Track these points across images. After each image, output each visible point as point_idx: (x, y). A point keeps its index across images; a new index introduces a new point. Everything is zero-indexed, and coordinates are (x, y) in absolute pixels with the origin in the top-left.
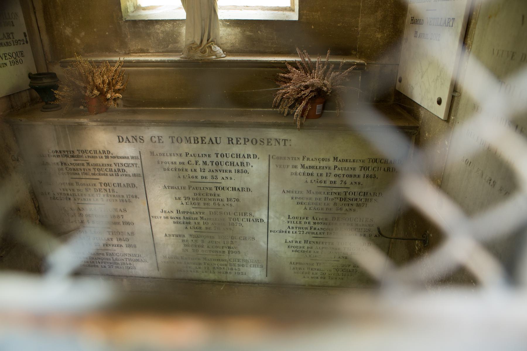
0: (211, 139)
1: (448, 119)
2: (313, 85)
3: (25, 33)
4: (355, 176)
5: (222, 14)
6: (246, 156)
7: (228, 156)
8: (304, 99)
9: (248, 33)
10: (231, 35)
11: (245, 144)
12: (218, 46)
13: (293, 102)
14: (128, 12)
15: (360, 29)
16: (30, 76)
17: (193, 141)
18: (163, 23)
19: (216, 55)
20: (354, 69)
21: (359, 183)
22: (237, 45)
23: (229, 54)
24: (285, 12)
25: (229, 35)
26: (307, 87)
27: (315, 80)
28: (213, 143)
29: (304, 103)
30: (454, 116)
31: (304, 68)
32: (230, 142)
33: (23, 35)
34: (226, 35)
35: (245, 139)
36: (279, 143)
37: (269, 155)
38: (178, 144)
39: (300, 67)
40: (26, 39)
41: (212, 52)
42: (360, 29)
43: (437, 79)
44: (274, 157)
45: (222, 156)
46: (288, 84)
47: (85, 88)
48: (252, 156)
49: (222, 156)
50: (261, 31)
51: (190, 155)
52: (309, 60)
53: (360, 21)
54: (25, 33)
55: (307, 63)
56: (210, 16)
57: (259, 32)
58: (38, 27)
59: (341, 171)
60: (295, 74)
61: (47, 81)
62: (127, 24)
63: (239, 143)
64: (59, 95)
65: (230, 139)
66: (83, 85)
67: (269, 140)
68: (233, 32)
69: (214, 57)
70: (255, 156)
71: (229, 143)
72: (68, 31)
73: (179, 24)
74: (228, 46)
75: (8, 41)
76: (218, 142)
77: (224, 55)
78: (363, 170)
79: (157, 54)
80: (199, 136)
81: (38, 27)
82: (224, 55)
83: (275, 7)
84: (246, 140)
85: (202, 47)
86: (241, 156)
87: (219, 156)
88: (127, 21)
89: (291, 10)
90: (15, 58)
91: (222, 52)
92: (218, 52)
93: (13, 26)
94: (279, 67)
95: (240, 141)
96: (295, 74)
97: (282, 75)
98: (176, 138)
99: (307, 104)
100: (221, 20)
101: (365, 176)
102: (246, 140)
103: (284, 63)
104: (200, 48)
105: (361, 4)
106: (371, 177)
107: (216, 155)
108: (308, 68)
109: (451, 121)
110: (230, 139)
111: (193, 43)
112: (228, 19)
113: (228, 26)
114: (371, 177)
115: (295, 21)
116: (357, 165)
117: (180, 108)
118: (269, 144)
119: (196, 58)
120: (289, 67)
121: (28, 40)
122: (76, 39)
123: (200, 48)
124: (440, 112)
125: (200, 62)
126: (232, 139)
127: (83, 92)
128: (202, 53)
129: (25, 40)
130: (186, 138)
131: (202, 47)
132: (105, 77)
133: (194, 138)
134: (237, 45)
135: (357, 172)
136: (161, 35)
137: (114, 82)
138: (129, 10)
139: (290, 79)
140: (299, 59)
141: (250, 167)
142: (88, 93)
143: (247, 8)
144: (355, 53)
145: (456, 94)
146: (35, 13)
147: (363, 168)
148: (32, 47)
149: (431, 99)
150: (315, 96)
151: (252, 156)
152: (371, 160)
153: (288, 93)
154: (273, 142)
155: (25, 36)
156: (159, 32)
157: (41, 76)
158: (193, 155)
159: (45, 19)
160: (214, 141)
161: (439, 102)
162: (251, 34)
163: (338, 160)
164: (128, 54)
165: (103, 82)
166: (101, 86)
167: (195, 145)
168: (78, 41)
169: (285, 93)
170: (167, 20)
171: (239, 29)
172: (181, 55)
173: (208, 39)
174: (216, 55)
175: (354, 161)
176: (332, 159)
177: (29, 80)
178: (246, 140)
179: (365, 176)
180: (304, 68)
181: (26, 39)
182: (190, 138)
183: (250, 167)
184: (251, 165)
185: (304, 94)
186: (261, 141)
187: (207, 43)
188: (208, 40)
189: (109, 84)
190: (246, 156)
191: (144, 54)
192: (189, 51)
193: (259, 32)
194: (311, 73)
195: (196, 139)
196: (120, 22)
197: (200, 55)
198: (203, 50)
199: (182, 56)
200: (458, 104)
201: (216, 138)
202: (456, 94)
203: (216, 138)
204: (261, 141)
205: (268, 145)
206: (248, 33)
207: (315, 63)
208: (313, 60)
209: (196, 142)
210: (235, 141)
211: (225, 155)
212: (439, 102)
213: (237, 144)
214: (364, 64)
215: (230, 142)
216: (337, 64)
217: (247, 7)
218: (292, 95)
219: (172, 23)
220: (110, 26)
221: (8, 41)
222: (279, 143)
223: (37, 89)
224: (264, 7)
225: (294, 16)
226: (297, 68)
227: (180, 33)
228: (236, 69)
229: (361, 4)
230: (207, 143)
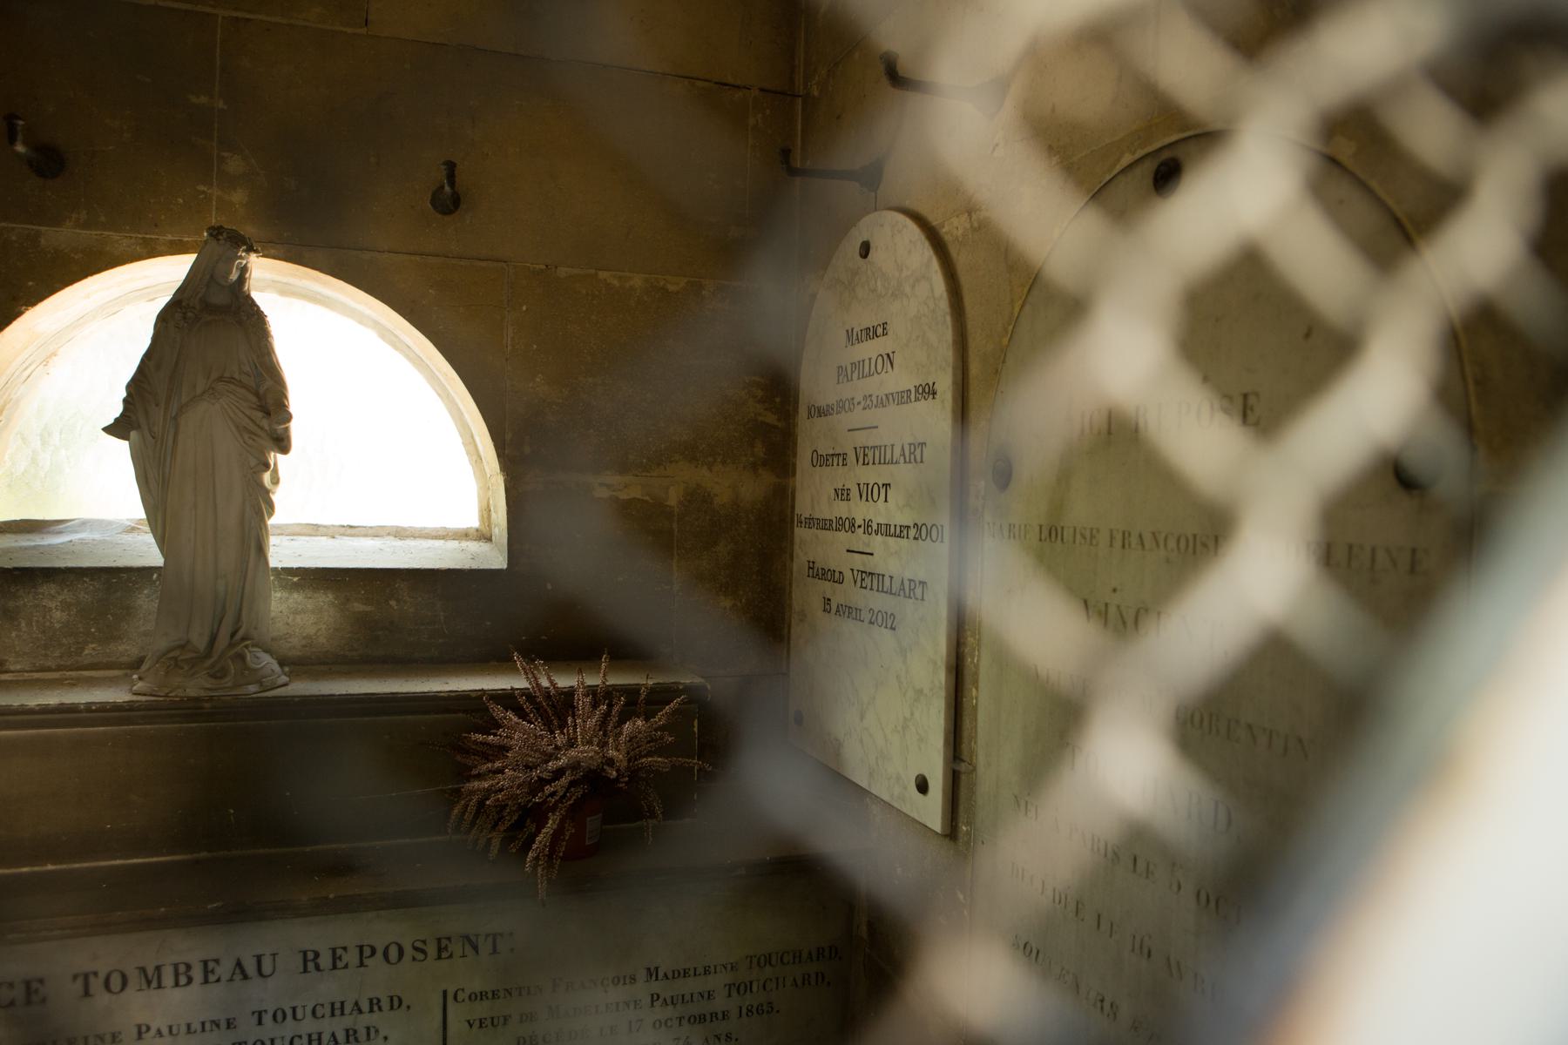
0: (239, 964)
1: (951, 832)
2: (575, 766)
4: (714, 1015)
5: (283, 553)
6: (365, 1006)
7: (299, 1016)
8: (553, 809)
9: (358, 607)
10: (303, 611)
11: (362, 964)
12: (266, 651)
13: (515, 818)
17: (168, 979)
21: (728, 1037)
24: (465, 544)
25: (296, 612)
26: (559, 773)
27: (580, 747)
28: (245, 977)
29: (551, 825)
30: (969, 824)
32: (311, 965)
35: (361, 948)
36: (475, 948)
37: (445, 993)
38: (107, 997)
39: (527, 707)
43: (905, 727)
44: (460, 996)
45: (279, 1016)
46: (498, 764)
48: (385, 1004)
49: (279, 1016)
50: (398, 601)
51: (153, 1031)
52: (551, 682)
55: (547, 695)
57: (393, 603)
59: (670, 1007)
60: (519, 733)
63: (340, 964)
65: (310, 956)
67: (444, 943)
69: (252, 688)
70: (396, 1003)
71: (305, 971)
76: (267, 969)
77: (284, 679)
78: (734, 993)
80: (195, 958)
82: (284, 679)
84: (365, 952)
86: (347, 1010)
87: (267, 1018)
89: (484, 536)
91: (276, 667)
94: (465, 711)
95: (346, 958)
96: (519, 733)
97: (480, 737)
98: (102, 976)
99: (562, 821)
100: (276, 569)
101: (744, 1011)
102: (367, 952)
103: (480, 698)
104: (209, 662)
105: (675, 526)
106: (760, 1010)
107: (255, 1019)
108: (557, 709)
109: (962, 838)
110: (310, 956)
111: (182, 647)
112: (295, 565)
113: (296, 587)
114: (760, 1010)
116: (717, 982)
117: (261, 851)
118: (444, 955)
120: (498, 711)
124: (931, 810)
125: (207, 705)
126: (317, 955)
128: (214, 676)
130: (143, 970)
133: (176, 966)
134: (322, 640)
135: (720, 1003)
136: (58, 614)
139: (503, 750)
140: (519, 683)
141: (380, 1040)
143: (350, 531)
145: (963, 767)
147: (735, 988)
149: (898, 778)
151: (385, 1004)
152: (755, 960)
153: (501, 790)
154: (456, 948)
156: (52, 605)
158: (165, 1031)
160: (250, 968)
161: (923, 786)
162: (368, 608)
163: (661, 975)
167: (178, 994)
171: (331, 596)
174: (261, 684)
175: (706, 971)
176: (642, 975)
178: (367, 952)
179: (744, 1011)
182: (158, 968)
183: (380, 1040)
184: (382, 1034)
185: (553, 794)
186: (416, 949)
187: (231, 645)
188: (233, 635)
190: (365, 1006)
193: (393, 603)
195: (182, 969)
197: (209, 683)
199: (140, 686)
200: (972, 791)
201: (259, 959)
202: (963, 767)
203: (259, 959)
204: (416, 949)
205: (439, 958)
207: (570, 693)
208: (565, 681)
209: (183, 980)
210: (325, 961)
211: (289, 1013)
212: (923, 786)
213: (334, 967)
215: (311, 965)
216: (631, 692)
217: (350, 530)
218: (514, 797)
222: (475, 948)
224: (404, 529)
225: (494, 558)
226: (522, 714)
229: (675, 526)
230: (224, 979)
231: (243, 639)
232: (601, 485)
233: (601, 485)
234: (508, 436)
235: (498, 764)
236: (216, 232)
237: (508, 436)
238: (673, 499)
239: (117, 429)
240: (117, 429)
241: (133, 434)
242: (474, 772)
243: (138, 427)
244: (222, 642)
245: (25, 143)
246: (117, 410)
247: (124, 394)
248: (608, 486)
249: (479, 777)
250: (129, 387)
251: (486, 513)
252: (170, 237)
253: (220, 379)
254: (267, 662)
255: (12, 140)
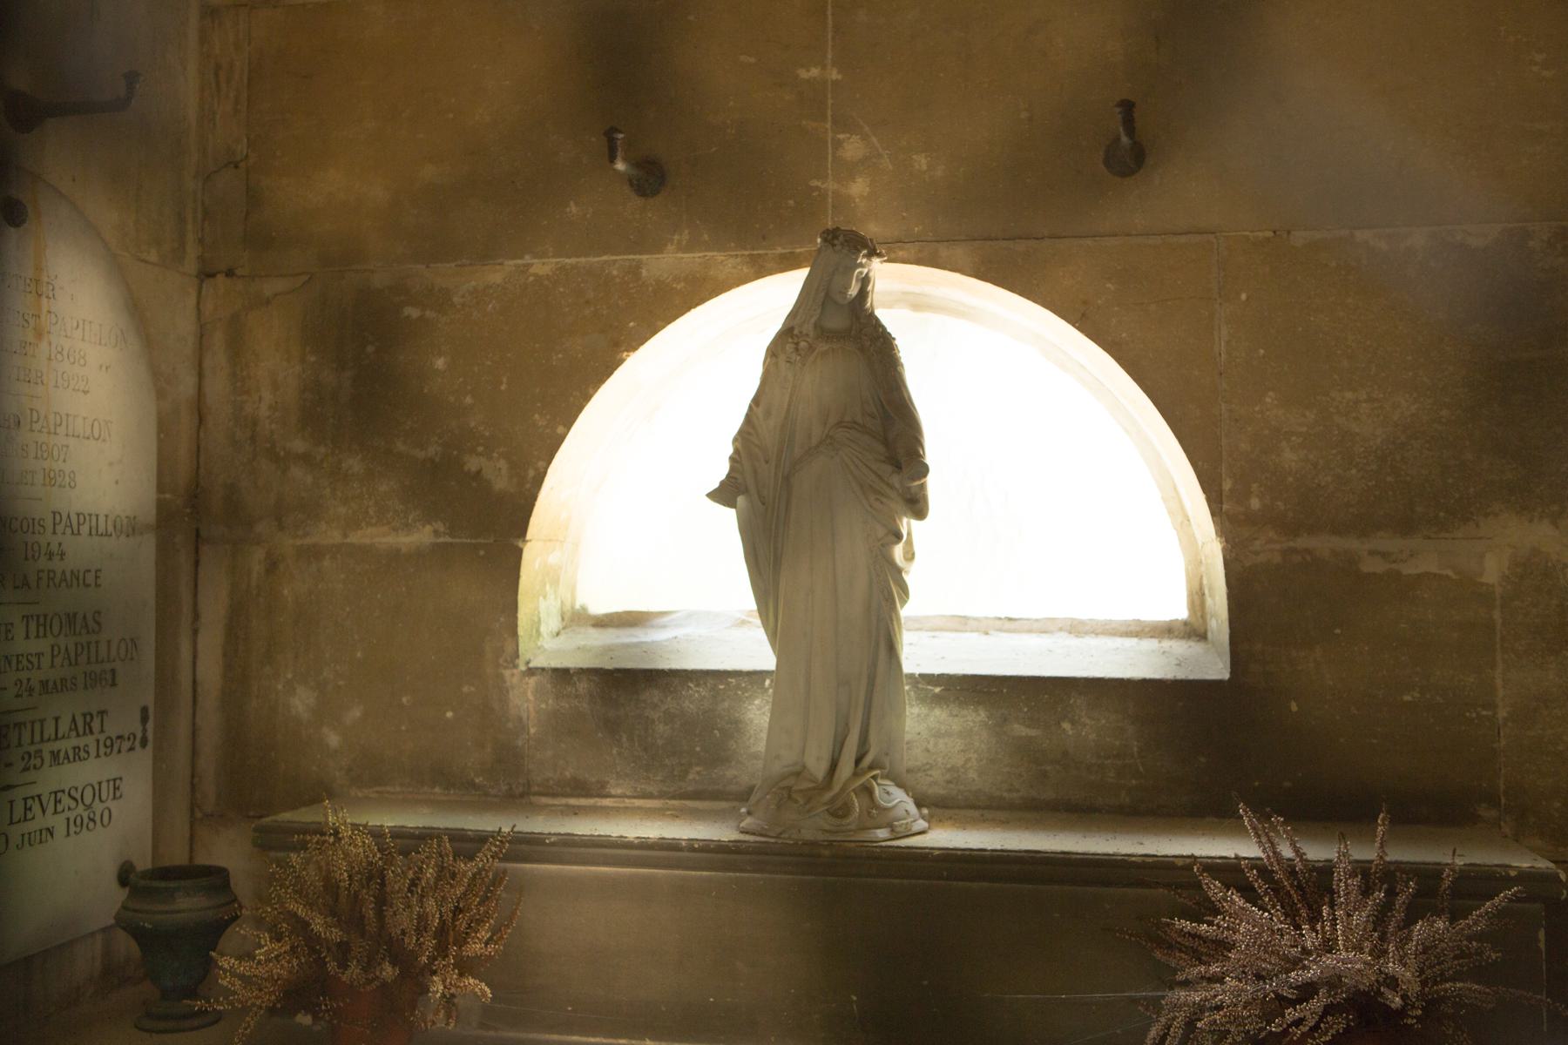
2: (1334, 982)
3: (145, 710)
5: (921, 653)
9: (1020, 730)
10: (948, 734)
12: (900, 785)
14: (539, 633)
15: (1502, 713)
16: (125, 876)
18: (676, 681)
19: (891, 826)
20: (1517, 899)
22: (972, 775)
23: (939, 811)
25: (938, 735)
26: (1307, 991)
31: (1276, 888)
33: (138, 716)
34: (919, 727)
39: (1260, 886)
40: (145, 730)
41: (877, 814)
42: (1502, 713)
46: (1215, 968)
47: (343, 950)
50: (1073, 723)
52: (1297, 851)
53: (1499, 682)
54: (145, 710)
55: (1292, 872)
56: (874, 665)
57: (1066, 725)
58: (194, 682)
61: (189, 906)
62: (532, 681)
64: (233, 975)
66: (336, 935)
68: (956, 725)
69: (882, 833)
72: (301, 702)
73: (738, 687)
74: (934, 782)
75: (81, 742)
79: (638, 803)
81: (194, 682)
83: (1126, 623)
85: (836, 788)
88: (531, 672)
89: (1193, 631)
90: (89, 807)
92: (900, 812)
93: (114, 684)
94: (1167, 886)
96: (1247, 923)
97: (1187, 925)
100: (911, 676)
103: (1189, 868)
104: (828, 796)
111: (798, 774)
112: (937, 671)
113: (938, 700)
115: (1221, 682)
119: (808, 834)
120: (1214, 889)
121: (150, 736)
122: (325, 730)
123: (828, 796)
127: (332, 966)
128: (834, 814)
129: (139, 735)
131: (836, 788)
132: (431, 905)
134: (972, 775)
137: (462, 923)
138: (543, 629)
139: (1221, 947)
142: (354, 972)
143: (1008, 625)
144: (1494, 813)
146: (195, 632)
148: (157, 759)
150: (1348, 1030)
153: (1218, 1008)
155: (144, 719)
156: (655, 715)
157: (172, 884)
159: (225, 655)
162: (1032, 732)
164: (522, 796)
165: (422, 925)
166: (410, 942)
168: (333, 740)
169: (1200, 1009)
170: (694, 672)
171: (983, 714)
172: (741, 818)
173: (861, 749)
174: (891, 826)
177: (122, 894)
180: (1276, 888)
181: (145, 730)
185: (1298, 1022)
187: (856, 775)
188: (858, 761)
189: (442, 931)
191: (583, 802)
192: (779, 807)
194: (1315, 918)
196: (507, 673)
198: (839, 803)
199: (748, 822)
206: (1020, 730)
207: (1325, 872)
214: (1556, 878)
217: (1010, 624)
218: (1236, 1020)
219: (711, 682)
220: (465, 689)
221: (81, 742)
223: (138, 934)
224: (1082, 622)
226: (1248, 892)
227: (736, 726)
228: (975, 885)
231: (871, 768)
232: (1371, 553)
233: (1371, 553)
234: (1227, 485)
235: (1215, 968)
236: (831, 236)
237: (1227, 485)
238: (1493, 570)
239: (724, 494)
240: (724, 494)
241: (740, 500)
242: (1180, 977)
243: (746, 491)
244: (846, 768)
245: (625, 160)
246: (721, 470)
247: (730, 450)
248: (1384, 555)
249: (1186, 984)
250: (735, 440)
251: (1198, 598)
252: (780, 250)
253: (839, 424)
254: (899, 800)
255: (612, 159)
